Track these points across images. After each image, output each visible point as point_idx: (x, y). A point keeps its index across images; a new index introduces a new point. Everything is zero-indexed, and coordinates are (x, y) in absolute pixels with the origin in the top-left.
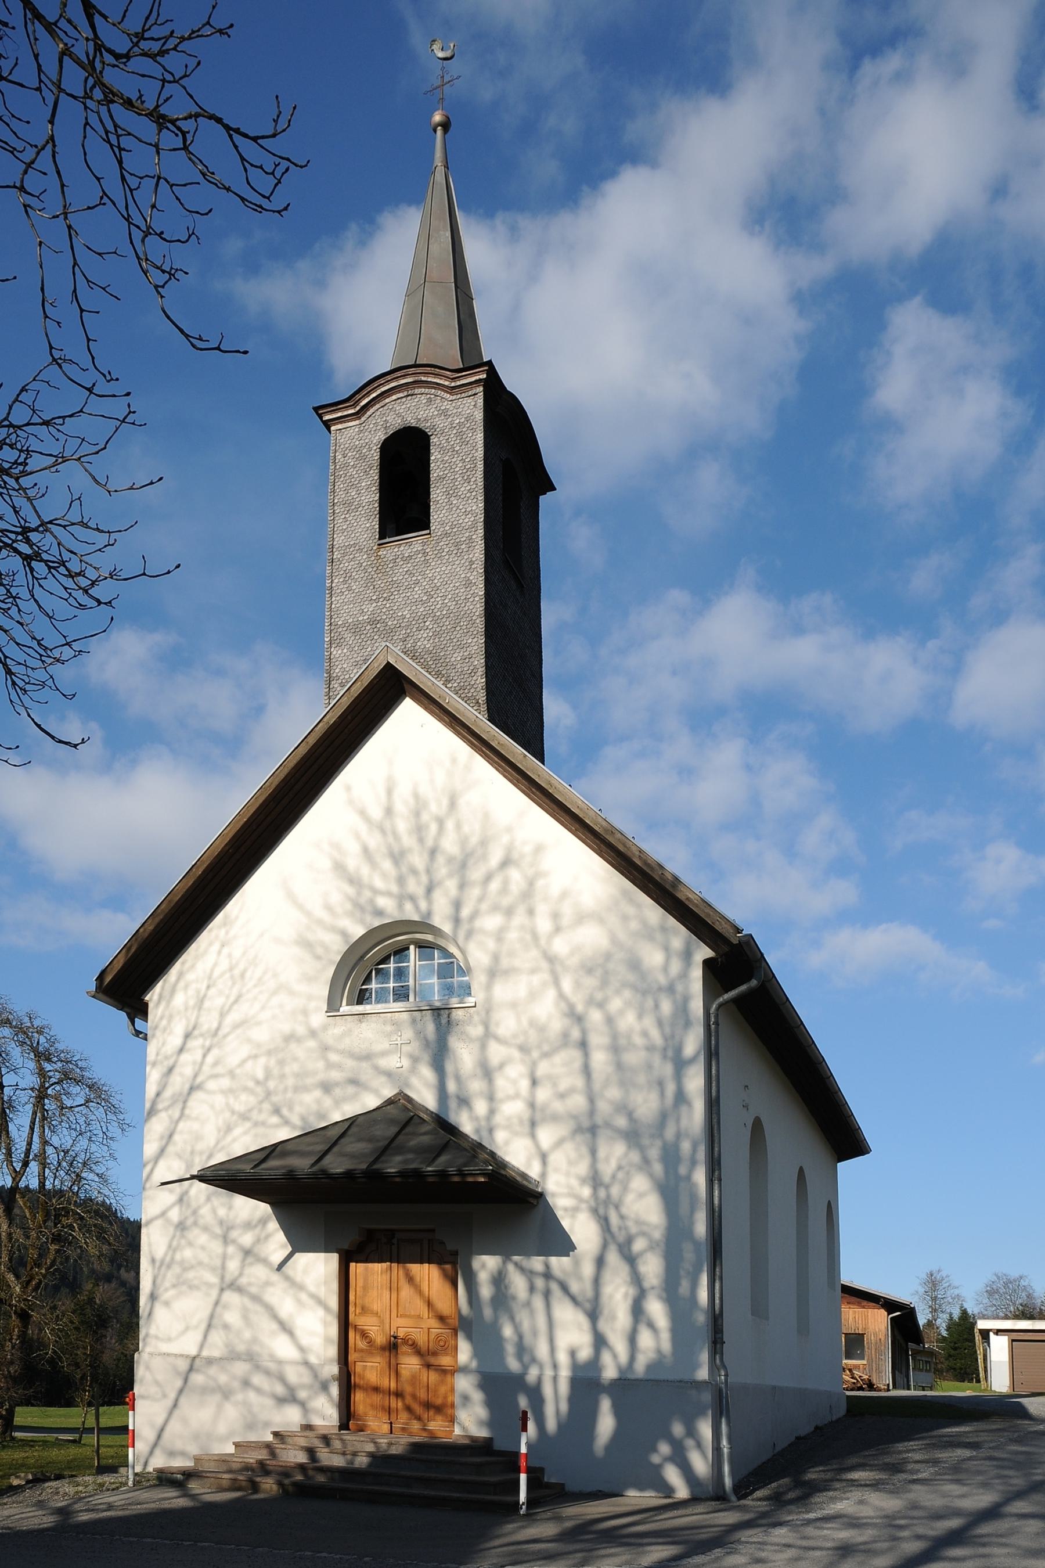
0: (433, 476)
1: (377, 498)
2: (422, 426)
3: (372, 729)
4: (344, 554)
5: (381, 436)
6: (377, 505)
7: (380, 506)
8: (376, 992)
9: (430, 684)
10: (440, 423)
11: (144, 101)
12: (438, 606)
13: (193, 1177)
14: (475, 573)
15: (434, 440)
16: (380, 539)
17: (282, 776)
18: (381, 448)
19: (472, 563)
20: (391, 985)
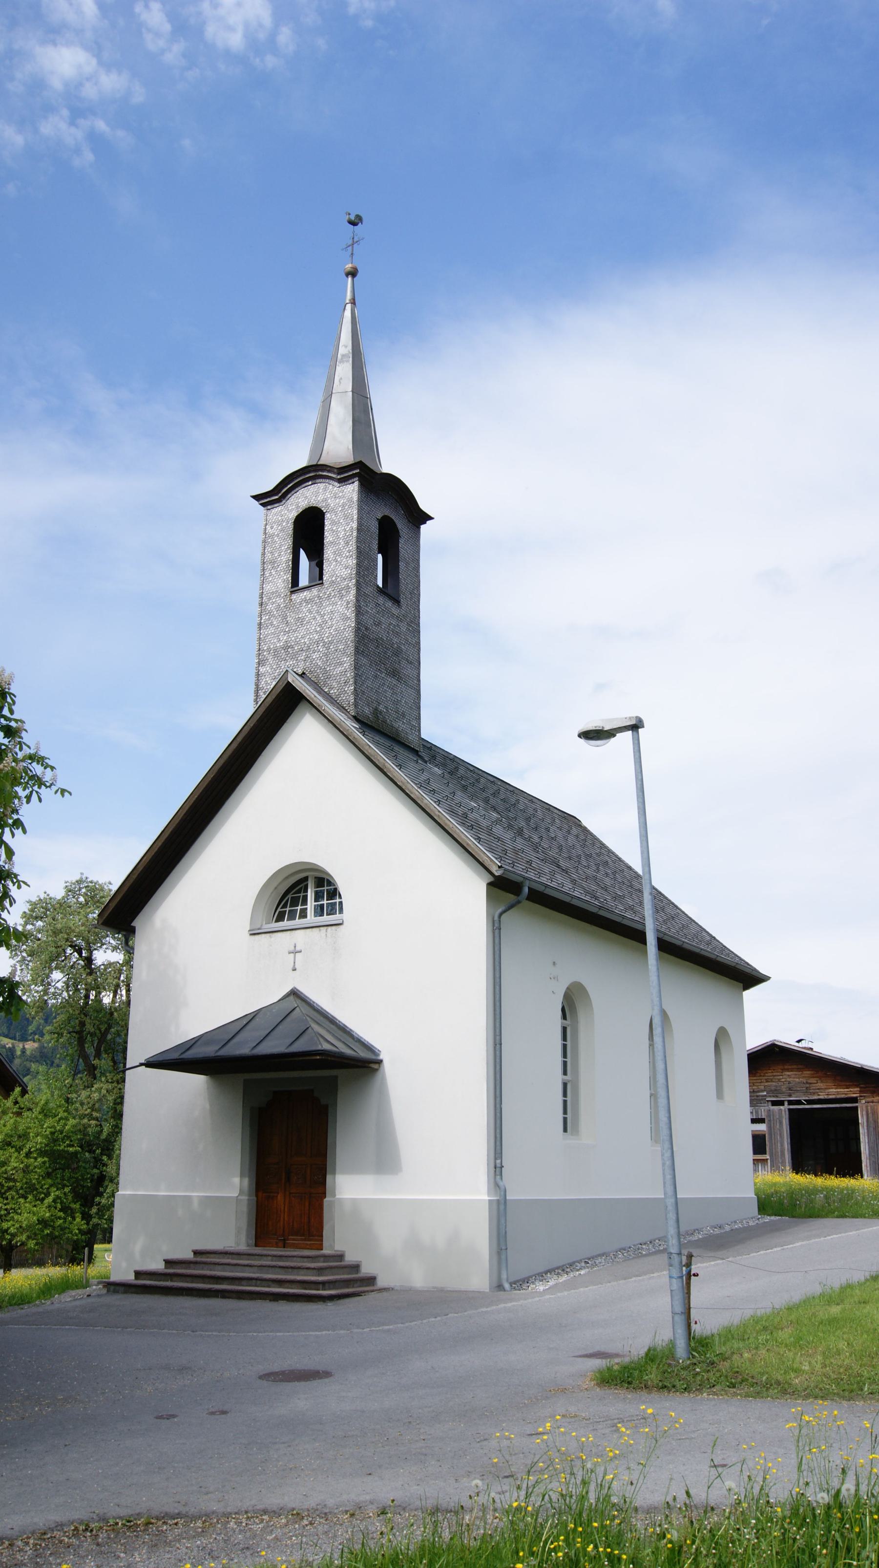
0: (326, 541)
1: (291, 558)
2: (319, 506)
3: (173, 833)
4: (270, 599)
5: (293, 514)
6: (290, 563)
7: (292, 564)
8: (327, 907)
9: (313, 696)
10: (332, 503)
11: (63, 795)
12: (326, 635)
13: (141, 1065)
14: (350, 610)
15: (327, 516)
16: (292, 587)
17: (192, 802)
18: (294, 522)
19: (348, 603)
20: (325, 902)
